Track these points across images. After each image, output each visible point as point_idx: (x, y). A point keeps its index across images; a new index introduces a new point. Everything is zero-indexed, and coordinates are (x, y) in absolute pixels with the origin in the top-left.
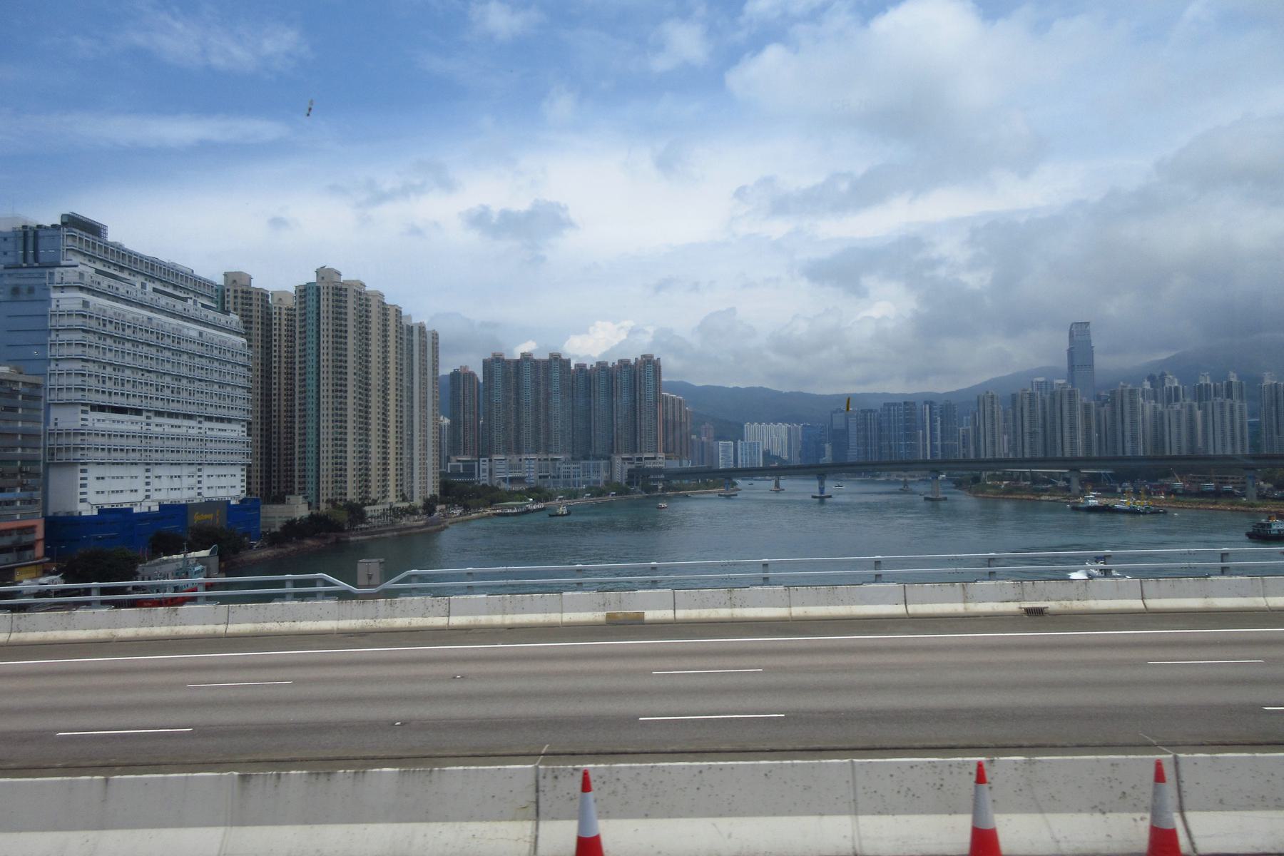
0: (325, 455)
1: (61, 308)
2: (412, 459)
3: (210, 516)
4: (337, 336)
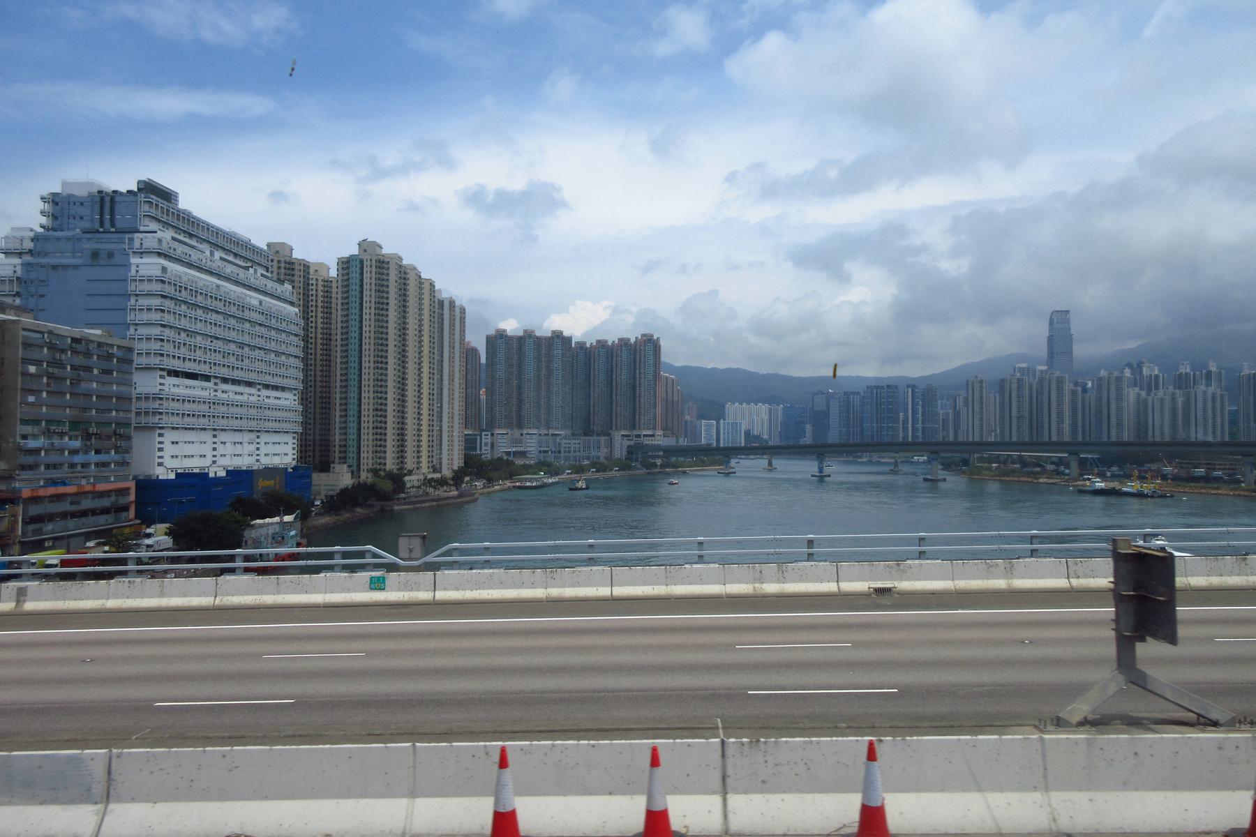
0: (366, 425)
1: (141, 273)
2: (441, 430)
3: (272, 482)
4: (378, 308)
